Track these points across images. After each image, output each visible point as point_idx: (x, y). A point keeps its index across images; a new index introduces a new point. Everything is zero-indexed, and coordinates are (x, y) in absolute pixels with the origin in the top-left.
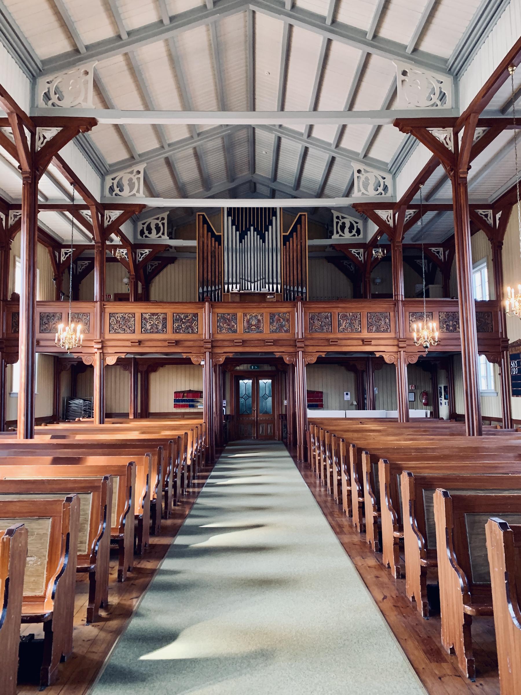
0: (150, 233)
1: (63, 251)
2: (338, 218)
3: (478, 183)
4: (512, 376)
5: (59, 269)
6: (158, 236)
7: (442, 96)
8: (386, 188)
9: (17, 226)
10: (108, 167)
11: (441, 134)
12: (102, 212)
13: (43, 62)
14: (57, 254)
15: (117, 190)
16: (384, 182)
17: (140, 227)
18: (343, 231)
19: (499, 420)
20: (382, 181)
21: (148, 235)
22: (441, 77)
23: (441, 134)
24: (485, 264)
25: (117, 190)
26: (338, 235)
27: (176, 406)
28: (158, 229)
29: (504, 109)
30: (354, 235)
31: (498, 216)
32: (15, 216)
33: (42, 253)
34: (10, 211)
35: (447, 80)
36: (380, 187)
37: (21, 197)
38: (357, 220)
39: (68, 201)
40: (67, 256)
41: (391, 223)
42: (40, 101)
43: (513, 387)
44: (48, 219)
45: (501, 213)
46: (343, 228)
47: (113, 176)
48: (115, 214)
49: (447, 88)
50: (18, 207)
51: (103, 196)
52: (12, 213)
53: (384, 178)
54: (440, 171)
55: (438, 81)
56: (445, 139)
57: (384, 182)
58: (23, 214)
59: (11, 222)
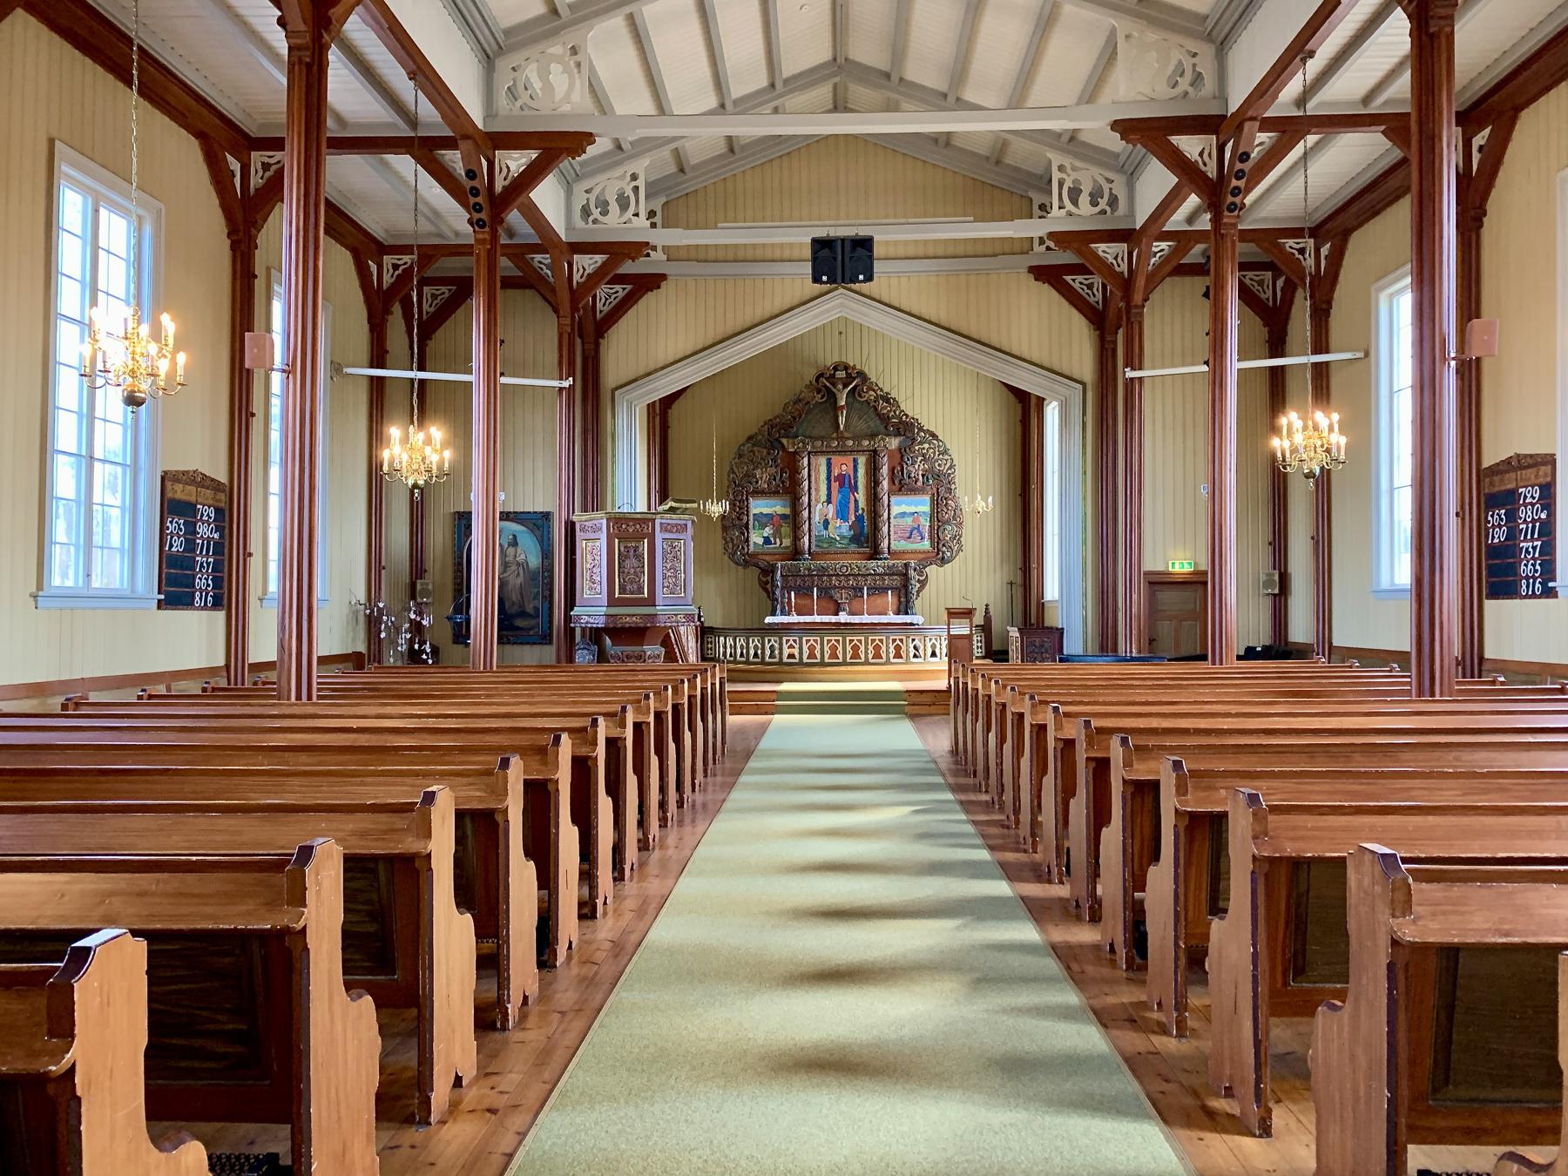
0: (605, 213)
1: (388, 260)
2: (1061, 168)
3: (1386, 103)
4: (1487, 546)
5: (378, 303)
6: (624, 219)
7: (1198, 78)
8: (1113, 202)
9: (273, 190)
10: (500, 37)
11: (1191, 145)
12: (489, 153)
13: (508, 32)
14: (374, 268)
15: (596, 213)
16: (1194, 65)
17: (579, 201)
18: (1075, 202)
19: (1401, 657)
20: (1106, 187)
21: (600, 218)
22: (1192, 45)
23: (1191, 145)
24: (1409, 280)
25: (596, 213)
26: (1043, 248)
27: (551, 643)
28: (623, 204)
29: (1301, 101)
30: (1103, 212)
31: (1325, 251)
32: (266, 167)
33: (337, 261)
34: (253, 154)
35: (1206, 51)
36: (1181, 75)
37: (283, 118)
38: (1111, 175)
39: (405, 131)
40: (268, 174)
41: (1124, 268)
42: (579, 223)
43: (1490, 575)
44: (347, 175)
45: (1487, 131)
46: (1074, 195)
47: (586, 185)
48: (515, 162)
49: (1207, 67)
50: (277, 144)
51: (569, 227)
52: (257, 158)
53: (1195, 55)
54: (1193, 200)
55: (1189, 52)
56: (1201, 154)
57: (1194, 65)
58: (290, 160)
59: (256, 181)
